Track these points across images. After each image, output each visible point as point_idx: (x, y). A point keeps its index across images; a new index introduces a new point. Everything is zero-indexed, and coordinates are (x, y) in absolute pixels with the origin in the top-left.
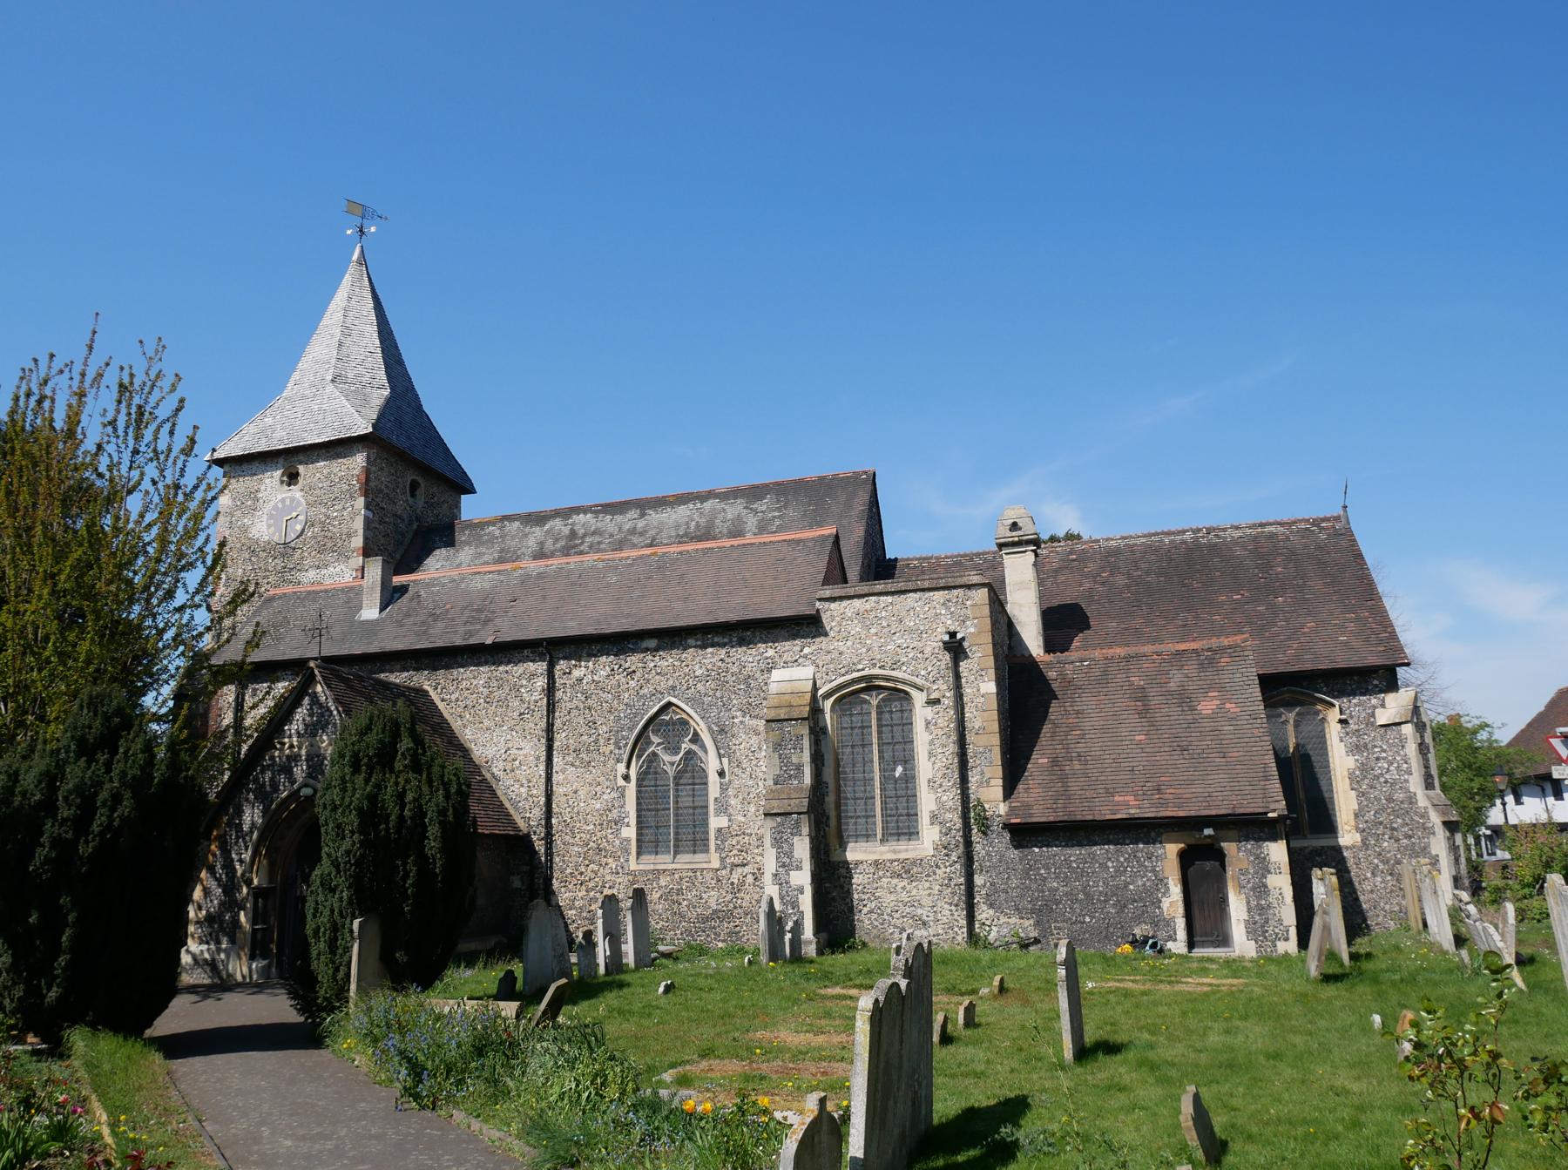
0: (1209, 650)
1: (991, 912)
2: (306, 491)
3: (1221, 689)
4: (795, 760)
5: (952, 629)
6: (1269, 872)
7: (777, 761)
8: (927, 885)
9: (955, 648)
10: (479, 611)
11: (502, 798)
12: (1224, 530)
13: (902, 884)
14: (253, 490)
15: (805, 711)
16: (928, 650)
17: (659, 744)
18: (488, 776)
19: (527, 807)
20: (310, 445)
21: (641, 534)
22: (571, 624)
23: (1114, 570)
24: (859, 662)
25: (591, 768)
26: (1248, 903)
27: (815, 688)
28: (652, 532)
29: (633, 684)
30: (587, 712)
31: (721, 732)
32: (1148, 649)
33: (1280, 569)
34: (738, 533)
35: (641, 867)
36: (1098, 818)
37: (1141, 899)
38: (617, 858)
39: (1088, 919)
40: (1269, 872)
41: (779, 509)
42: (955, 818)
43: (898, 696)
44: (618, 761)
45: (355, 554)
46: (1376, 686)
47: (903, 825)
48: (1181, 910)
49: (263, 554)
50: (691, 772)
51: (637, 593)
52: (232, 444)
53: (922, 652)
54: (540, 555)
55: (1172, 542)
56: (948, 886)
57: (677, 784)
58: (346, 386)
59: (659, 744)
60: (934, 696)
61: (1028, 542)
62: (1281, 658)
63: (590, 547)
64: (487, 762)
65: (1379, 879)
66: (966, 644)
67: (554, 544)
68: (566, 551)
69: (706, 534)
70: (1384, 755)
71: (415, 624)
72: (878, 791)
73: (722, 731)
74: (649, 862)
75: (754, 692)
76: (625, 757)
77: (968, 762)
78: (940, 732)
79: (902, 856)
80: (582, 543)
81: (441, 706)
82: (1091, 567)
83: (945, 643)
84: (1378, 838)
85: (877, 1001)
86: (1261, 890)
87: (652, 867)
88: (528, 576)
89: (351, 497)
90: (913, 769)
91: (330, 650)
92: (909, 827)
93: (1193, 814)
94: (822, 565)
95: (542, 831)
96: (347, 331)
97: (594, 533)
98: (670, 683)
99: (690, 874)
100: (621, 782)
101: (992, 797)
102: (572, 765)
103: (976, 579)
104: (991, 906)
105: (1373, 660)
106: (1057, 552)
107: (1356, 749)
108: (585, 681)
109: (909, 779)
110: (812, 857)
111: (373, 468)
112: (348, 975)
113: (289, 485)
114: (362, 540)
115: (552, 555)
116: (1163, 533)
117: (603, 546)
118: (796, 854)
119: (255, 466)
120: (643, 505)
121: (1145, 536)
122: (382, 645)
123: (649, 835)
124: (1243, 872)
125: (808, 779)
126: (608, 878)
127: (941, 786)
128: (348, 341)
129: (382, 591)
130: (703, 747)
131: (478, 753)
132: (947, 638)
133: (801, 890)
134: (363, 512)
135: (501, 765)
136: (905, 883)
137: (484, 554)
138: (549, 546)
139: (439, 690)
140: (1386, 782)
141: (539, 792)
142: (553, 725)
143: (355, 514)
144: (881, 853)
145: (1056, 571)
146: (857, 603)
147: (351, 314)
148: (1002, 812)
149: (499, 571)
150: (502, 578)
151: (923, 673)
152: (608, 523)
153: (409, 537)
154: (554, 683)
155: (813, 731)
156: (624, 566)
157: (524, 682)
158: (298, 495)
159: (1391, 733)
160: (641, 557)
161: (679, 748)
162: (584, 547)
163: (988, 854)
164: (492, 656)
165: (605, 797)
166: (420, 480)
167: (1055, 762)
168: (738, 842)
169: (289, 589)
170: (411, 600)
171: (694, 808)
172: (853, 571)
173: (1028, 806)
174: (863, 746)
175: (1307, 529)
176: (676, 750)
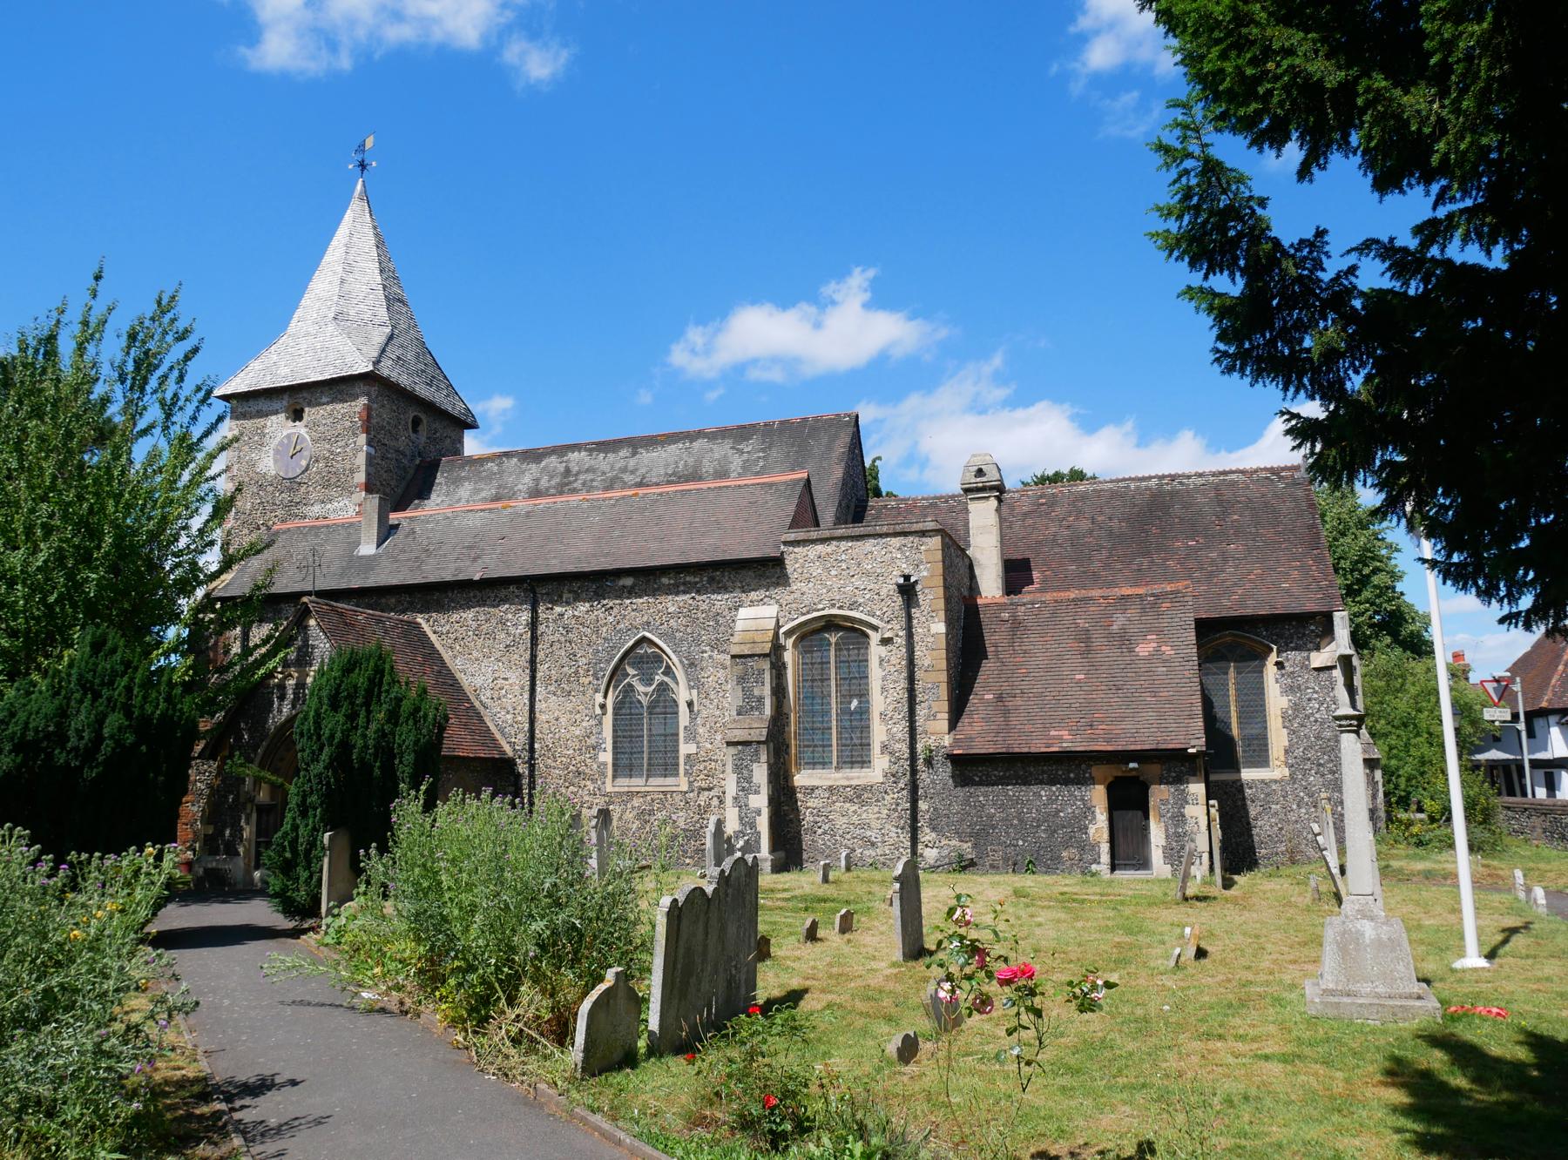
0: (1152, 595)
1: (934, 835)
3: (1159, 632)
4: (756, 692)
5: (907, 572)
6: (1187, 803)
7: (740, 694)
8: (876, 809)
9: (907, 590)
12: (1189, 477)
13: (853, 808)
15: (767, 648)
16: (884, 592)
17: (634, 676)
18: (477, 704)
21: (632, 472)
22: (554, 562)
23: (1079, 514)
24: (820, 603)
26: (1167, 830)
27: (778, 626)
28: (643, 471)
29: (611, 619)
31: (691, 665)
32: (1096, 593)
33: (1236, 517)
34: (722, 474)
35: (617, 789)
36: (1033, 750)
37: (1070, 825)
38: (594, 781)
39: (1021, 843)
40: (1187, 803)
41: (763, 450)
42: (903, 748)
43: (853, 632)
44: (597, 691)
46: (1313, 631)
47: (857, 755)
48: (1106, 836)
49: (270, 489)
50: (664, 703)
51: (617, 533)
53: (878, 594)
54: (536, 493)
55: (1138, 488)
56: (895, 810)
57: (650, 713)
58: (349, 323)
59: (634, 676)
60: (887, 635)
61: (992, 488)
62: (1225, 602)
63: (584, 484)
65: (1303, 810)
66: (918, 588)
68: (561, 489)
69: (695, 476)
70: (1315, 696)
71: (409, 560)
72: (834, 723)
73: (692, 665)
74: (624, 784)
75: (722, 628)
76: (603, 688)
78: (893, 669)
79: (854, 783)
81: (433, 638)
82: (1059, 511)
83: (899, 586)
84: (1305, 773)
85: (675, 900)
86: (1179, 818)
87: (626, 789)
88: (517, 514)
90: (868, 702)
91: (323, 584)
92: (862, 756)
93: (1120, 748)
94: (791, 509)
95: (526, 755)
96: (348, 268)
97: (587, 471)
98: (645, 619)
99: (661, 796)
100: (598, 711)
101: (938, 729)
103: (931, 525)
104: (934, 829)
105: (1311, 606)
106: (1028, 496)
107: (1289, 690)
109: (864, 711)
110: (770, 782)
111: (375, 406)
112: (320, 880)
116: (1130, 479)
117: (595, 484)
118: (755, 780)
119: (263, 404)
120: (636, 444)
121: (1112, 481)
122: (379, 579)
123: (624, 761)
124: (1164, 802)
125: (768, 710)
126: (586, 798)
127: (891, 718)
128: (350, 278)
129: (379, 527)
130: (674, 678)
131: (465, 681)
132: (901, 581)
133: (759, 813)
135: (488, 693)
136: (856, 807)
137: (482, 490)
138: (544, 483)
140: (1316, 721)
141: (524, 718)
143: (357, 450)
144: (835, 780)
145: (1025, 514)
146: (819, 548)
148: (947, 744)
149: (490, 509)
150: (492, 516)
151: (878, 613)
152: (603, 462)
153: (412, 472)
154: (537, 618)
155: (773, 666)
156: (606, 506)
157: (510, 616)
159: (1324, 676)
160: (623, 498)
161: (653, 680)
162: (577, 485)
163: (933, 782)
165: (584, 724)
166: (423, 416)
167: (1000, 698)
168: (705, 768)
169: (298, 523)
170: (407, 536)
171: (665, 736)
172: (827, 513)
173: (971, 739)
174: (822, 681)
175: (1267, 478)
176: (649, 682)
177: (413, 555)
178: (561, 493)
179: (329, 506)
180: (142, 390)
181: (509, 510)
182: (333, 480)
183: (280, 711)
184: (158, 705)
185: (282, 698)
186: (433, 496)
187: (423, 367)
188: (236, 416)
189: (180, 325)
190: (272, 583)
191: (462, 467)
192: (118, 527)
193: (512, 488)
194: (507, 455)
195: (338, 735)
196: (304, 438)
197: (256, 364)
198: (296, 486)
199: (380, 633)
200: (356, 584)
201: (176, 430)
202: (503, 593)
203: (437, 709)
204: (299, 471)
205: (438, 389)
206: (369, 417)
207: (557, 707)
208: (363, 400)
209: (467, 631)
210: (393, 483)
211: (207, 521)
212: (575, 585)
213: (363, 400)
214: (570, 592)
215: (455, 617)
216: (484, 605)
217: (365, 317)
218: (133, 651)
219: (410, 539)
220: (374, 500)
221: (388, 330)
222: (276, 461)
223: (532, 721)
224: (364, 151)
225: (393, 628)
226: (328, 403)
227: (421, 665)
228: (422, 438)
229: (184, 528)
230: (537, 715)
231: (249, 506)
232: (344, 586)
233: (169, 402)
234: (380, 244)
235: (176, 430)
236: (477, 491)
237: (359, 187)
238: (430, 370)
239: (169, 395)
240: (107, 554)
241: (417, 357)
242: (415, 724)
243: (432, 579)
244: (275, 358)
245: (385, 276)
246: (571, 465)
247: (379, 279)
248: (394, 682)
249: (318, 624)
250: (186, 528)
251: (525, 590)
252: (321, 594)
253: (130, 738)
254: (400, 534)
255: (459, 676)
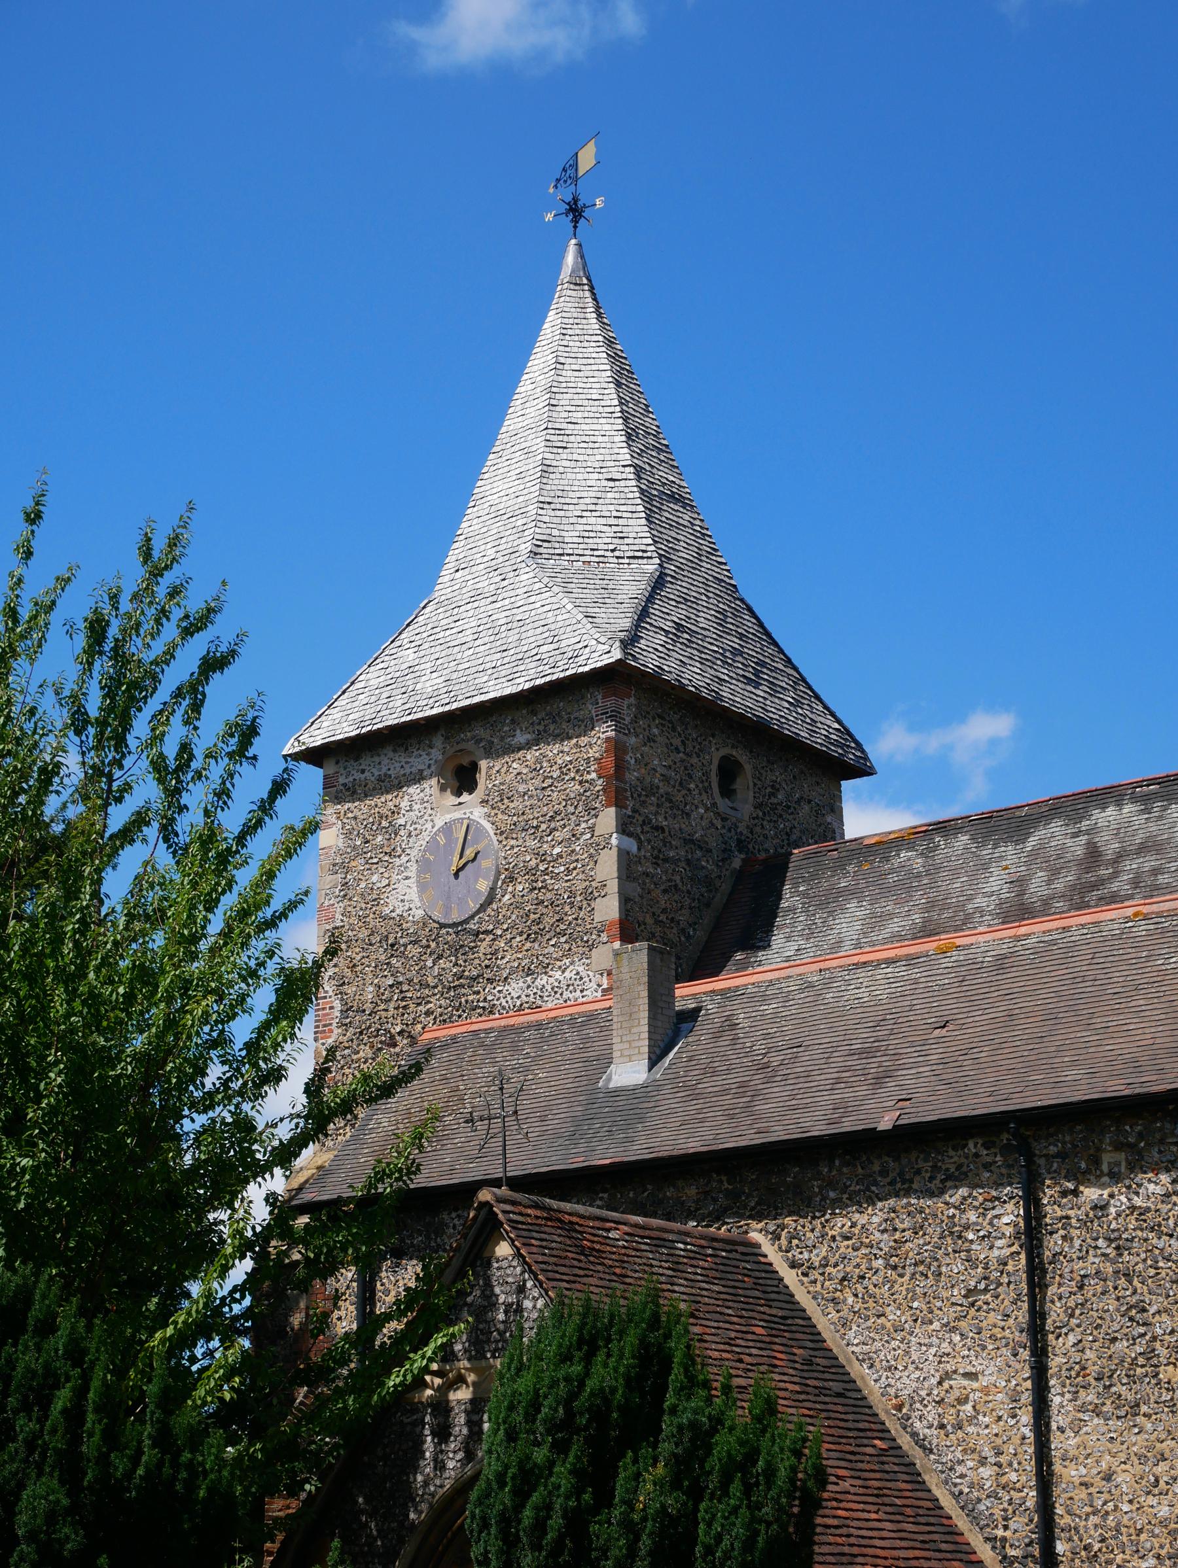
2: (497, 801)
10: (866, 1053)
11: (938, 1492)
14: (384, 811)
18: (905, 1441)
19: (998, 1513)
20: (465, 710)
22: (1072, 1074)
25: (1139, 1420)
30: (1122, 1282)
45: (604, 937)
49: (413, 951)
52: (335, 713)
63: (1136, 883)
64: (899, 1407)
67: (1049, 882)
68: (1079, 899)
71: (725, 1092)
77: (1032, 1355)
80: (1116, 874)
81: (790, 1277)
88: (975, 966)
89: (588, 810)
91: (522, 1163)
97: (1142, 849)
102: (1097, 1411)
108: (1113, 1210)
113: (458, 794)
114: (616, 904)
115: (1044, 909)
117: (1163, 879)
119: (390, 763)
122: (655, 1142)
128: (562, 460)
129: (653, 1018)
134: (614, 841)
135: (931, 1416)
137: (891, 915)
138: (1037, 886)
139: (784, 1242)
141: (1023, 1475)
142: (1043, 1316)
143: (601, 846)
147: (564, 400)
149: (909, 958)
150: (915, 973)
153: (725, 887)
154: (1040, 1216)
157: (972, 1216)
158: (478, 814)
162: (1120, 885)
164: (897, 1159)
169: (479, 1023)
170: (717, 1035)
177: (733, 1079)
178: (1082, 906)
179: (542, 980)
180: (120, 741)
181: (955, 955)
182: (548, 921)
183: (440, 1466)
184: (139, 1452)
185: (443, 1433)
186: (777, 940)
187: (736, 643)
188: (336, 792)
189: (194, 603)
190: (414, 1169)
191: (840, 865)
192: (79, 1049)
193: (961, 906)
194: (944, 828)
195: (556, 1522)
196: (480, 830)
197: (372, 678)
198: (468, 940)
199: (663, 1269)
200: (604, 1155)
201: (189, 823)
202: (952, 1159)
203: (798, 1454)
204: (473, 906)
205: (774, 690)
206: (620, 767)
207: (1104, 1444)
208: (605, 731)
209: (869, 1259)
210: (683, 917)
211: (266, 1026)
212: (1132, 1131)
213: (605, 731)
214: (1118, 1147)
215: (840, 1224)
216: (908, 1193)
217: (600, 543)
218: (89, 1327)
219: (724, 1042)
220: (639, 956)
221: (651, 567)
222: (422, 887)
223: (1045, 1481)
224: (575, 180)
225: (693, 1256)
226: (528, 746)
227: (765, 1345)
228: (745, 807)
229: (215, 1044)
230: (1057, 1467)
231: (370, 993)
232: (577, 1161)
233: (172, 764)
234: (623, 377)
235: (189, 823)
236: (877, 920)
237: (570, 258)
238: (752, 650)
239: (170, 749)
240: (53, 1111)
241: (722, 622)
242: (748, 1490)
243: (779, 1133)
244: (410, 656)
245: (637, 446)
246: (1102, 839)
247: (625, 455)
248: (694, 1383)
249: (518, 1254)
250: (222, 1041)
251: (1006, 1150)
252: (520, 1183)
253: (71, 1538)
254: (701, 1034)
255: (858, 1370)
